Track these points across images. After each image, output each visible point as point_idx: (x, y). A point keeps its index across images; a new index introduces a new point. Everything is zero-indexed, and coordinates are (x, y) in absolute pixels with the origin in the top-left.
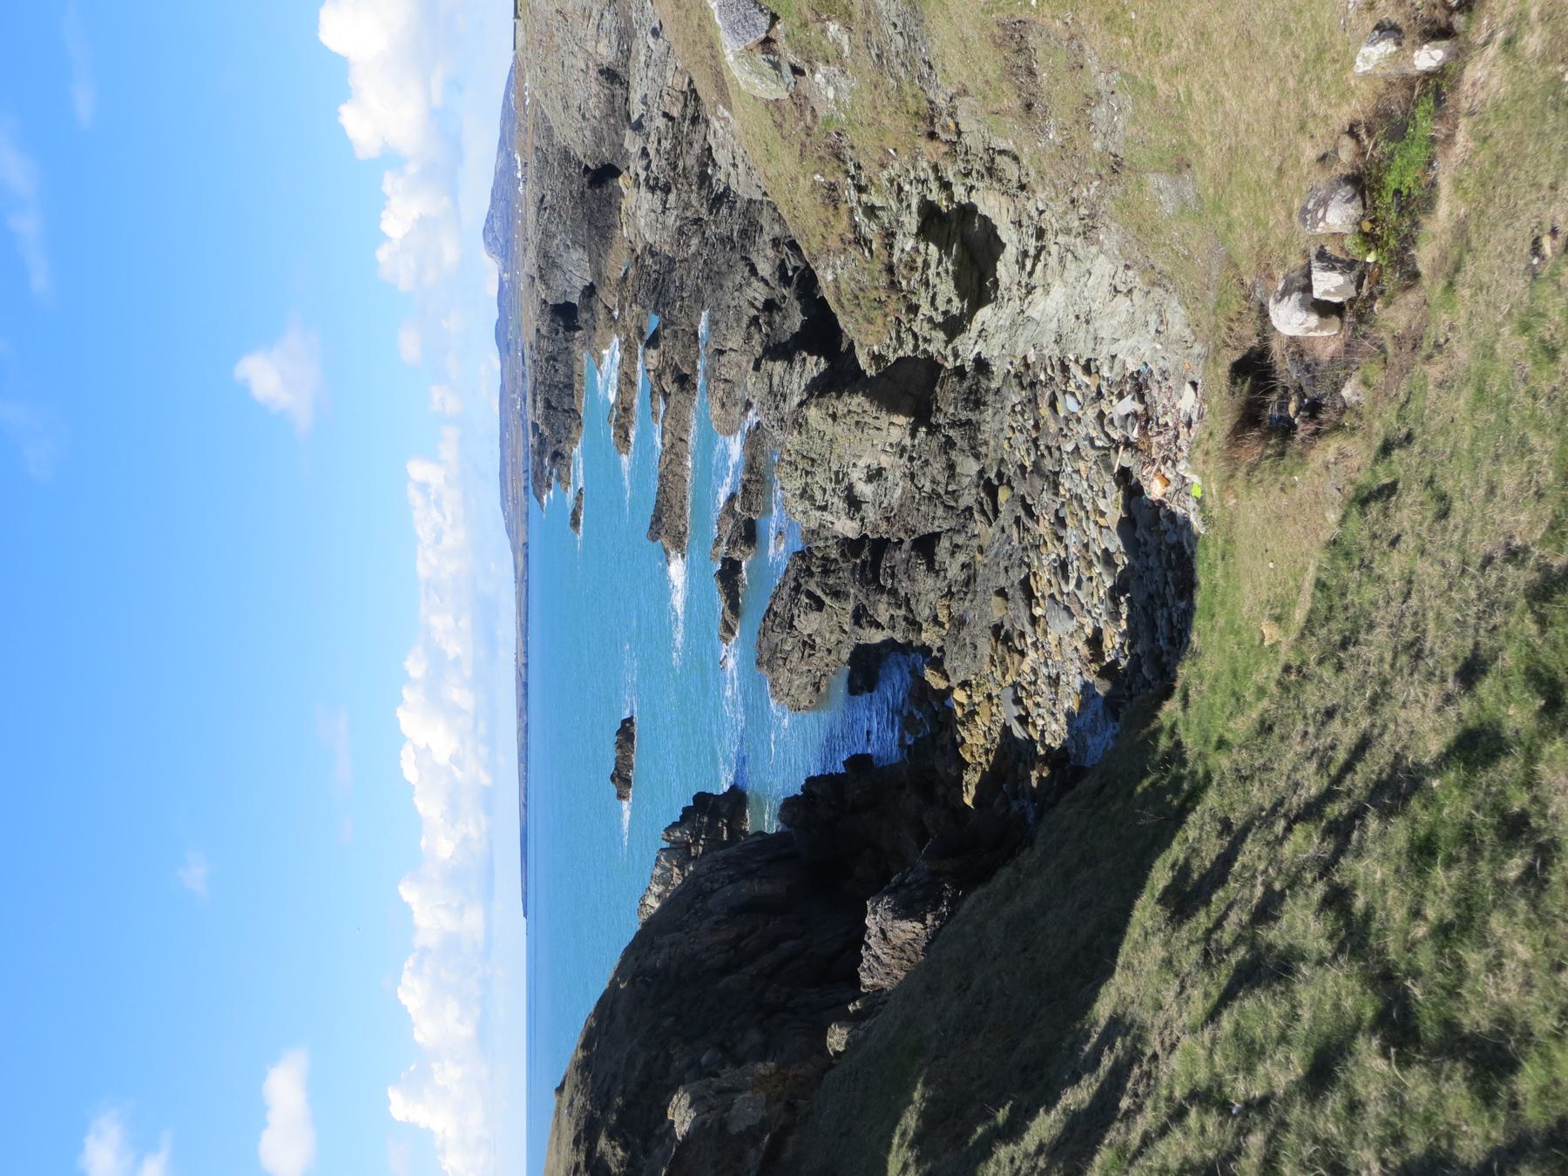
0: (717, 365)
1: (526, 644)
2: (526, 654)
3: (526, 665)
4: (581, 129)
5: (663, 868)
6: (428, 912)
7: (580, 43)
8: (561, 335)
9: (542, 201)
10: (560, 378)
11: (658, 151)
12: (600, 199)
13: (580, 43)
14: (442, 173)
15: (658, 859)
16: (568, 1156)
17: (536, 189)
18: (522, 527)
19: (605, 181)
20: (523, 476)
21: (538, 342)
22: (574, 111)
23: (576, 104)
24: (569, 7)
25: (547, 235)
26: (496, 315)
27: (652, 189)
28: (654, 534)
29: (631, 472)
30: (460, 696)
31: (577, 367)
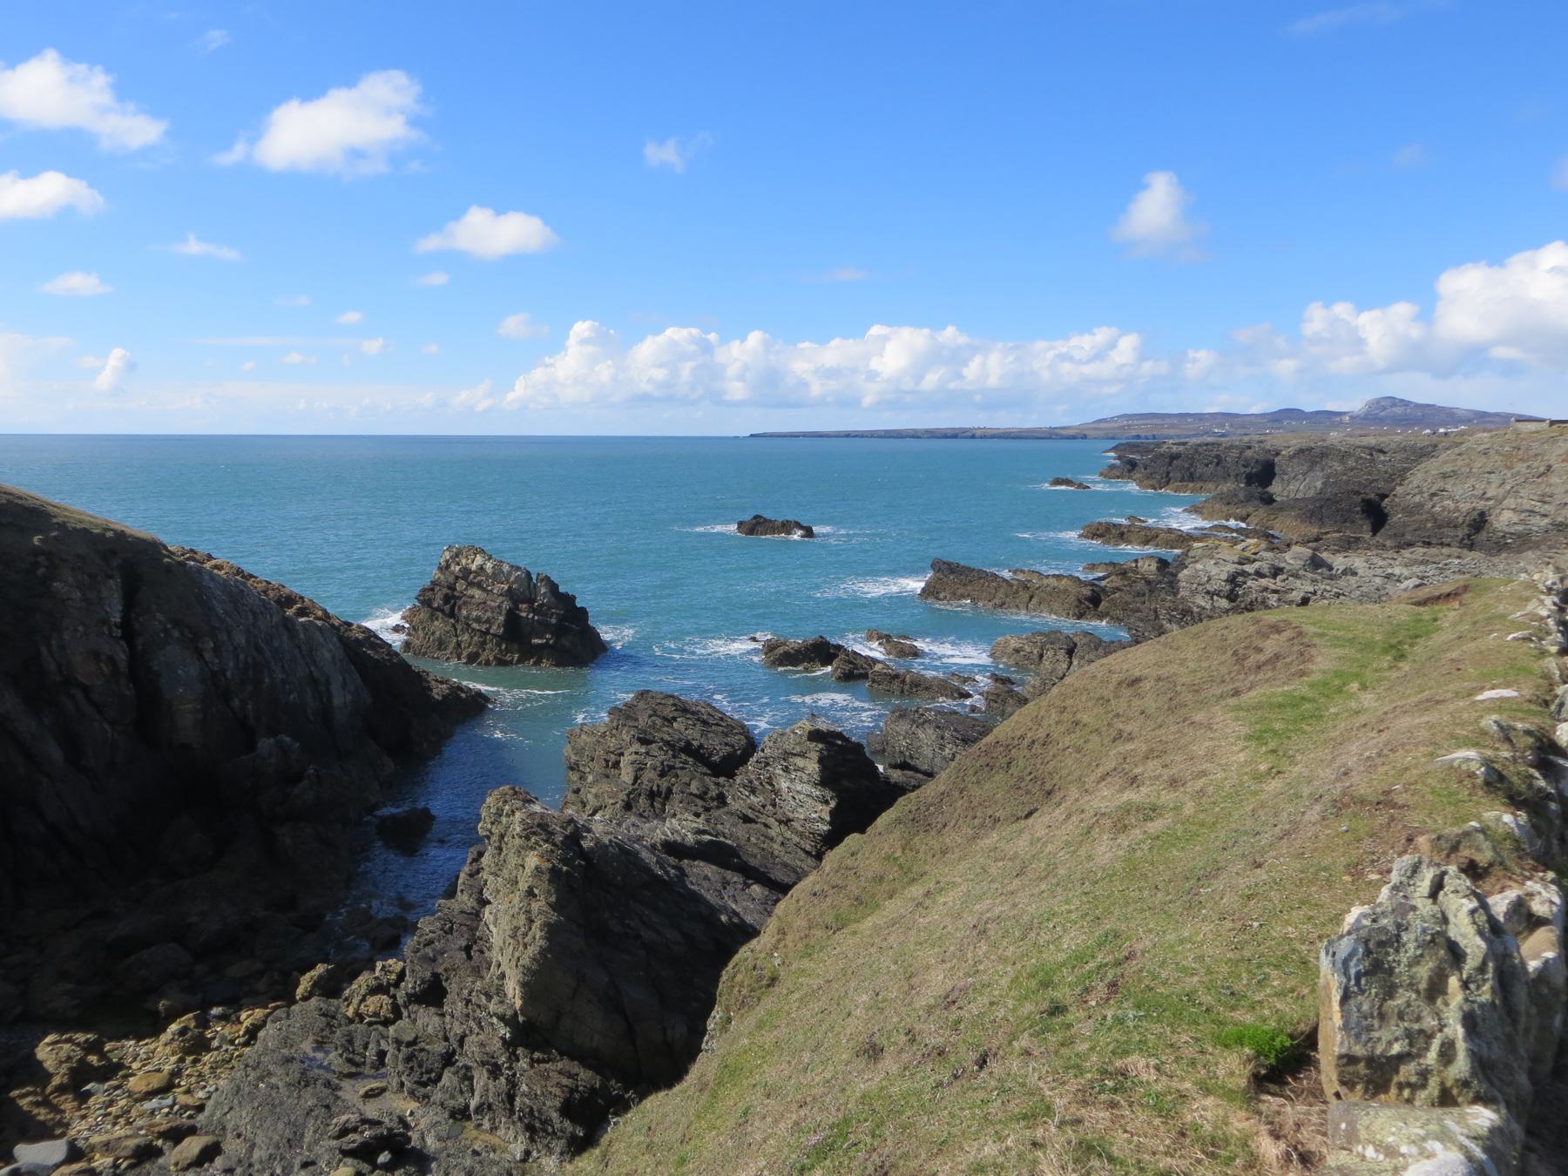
0: (1057, 646)
1: (993, 437)
2: (983, 437)
3: (973, 437)
4: (1421, 492)
5: (509, 573)
6: (744, 351)
7: (1514, 492)
9: (1382, 451)
11: (1266, 589)
12: (1349, 511)
13: (1514, 492)
15: (518, 568)
17: (1393, 446)
18: (1101, 433)
19: (1368, 517)
20: (1149, 434)
21: (1237, 447)
22: (1440, 484)
23: (1448, 487)
24: (1554, 479)
25: (1344, 456)
26: (1308, 409)
27: (1232, 580)
28: (937, 565)
29: (1060, 542)
30: (931, 380)
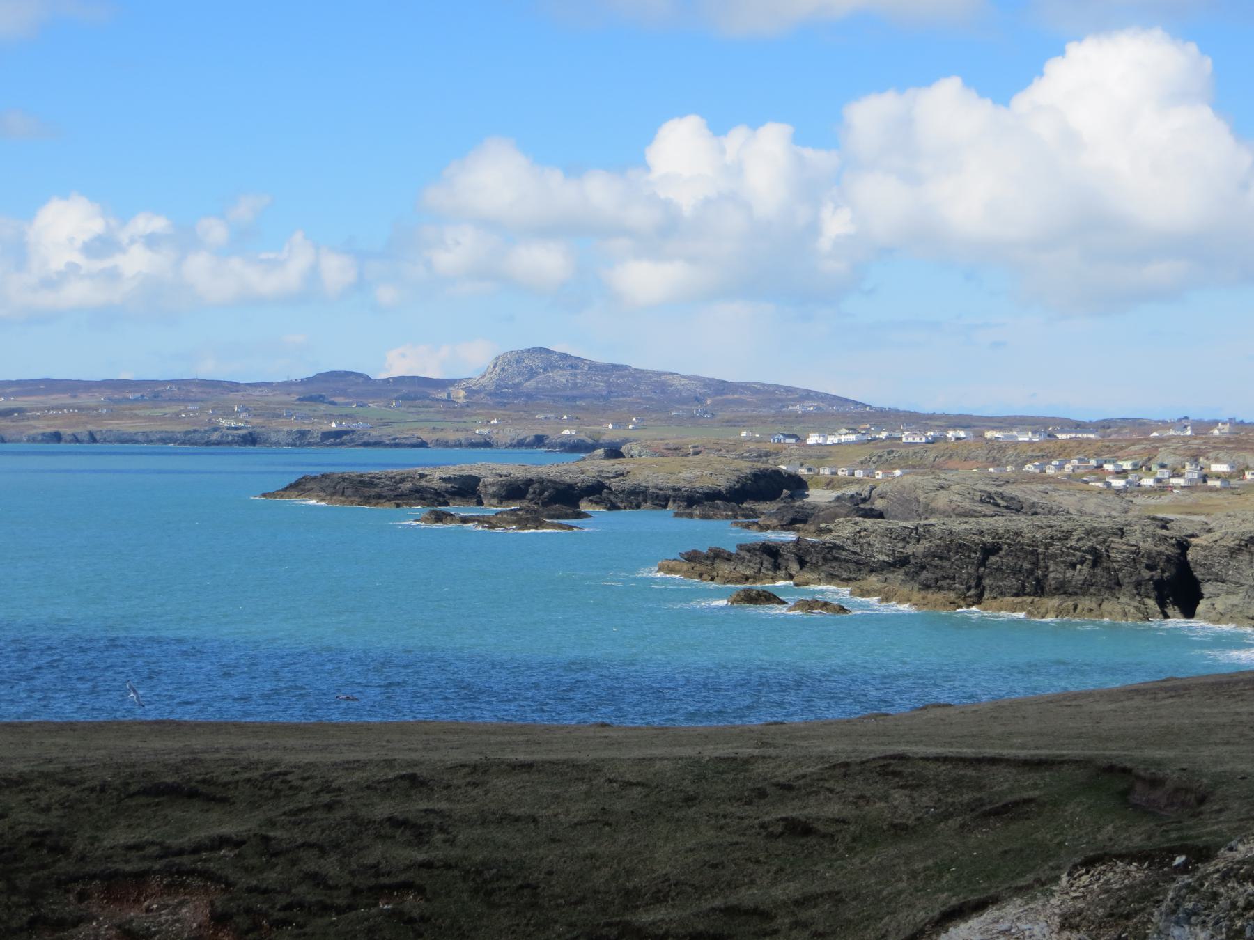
8: (1146, 574)
10: (1055, 574)
14: (778, 271)
16: (18, 759)
31: (1086, 603)
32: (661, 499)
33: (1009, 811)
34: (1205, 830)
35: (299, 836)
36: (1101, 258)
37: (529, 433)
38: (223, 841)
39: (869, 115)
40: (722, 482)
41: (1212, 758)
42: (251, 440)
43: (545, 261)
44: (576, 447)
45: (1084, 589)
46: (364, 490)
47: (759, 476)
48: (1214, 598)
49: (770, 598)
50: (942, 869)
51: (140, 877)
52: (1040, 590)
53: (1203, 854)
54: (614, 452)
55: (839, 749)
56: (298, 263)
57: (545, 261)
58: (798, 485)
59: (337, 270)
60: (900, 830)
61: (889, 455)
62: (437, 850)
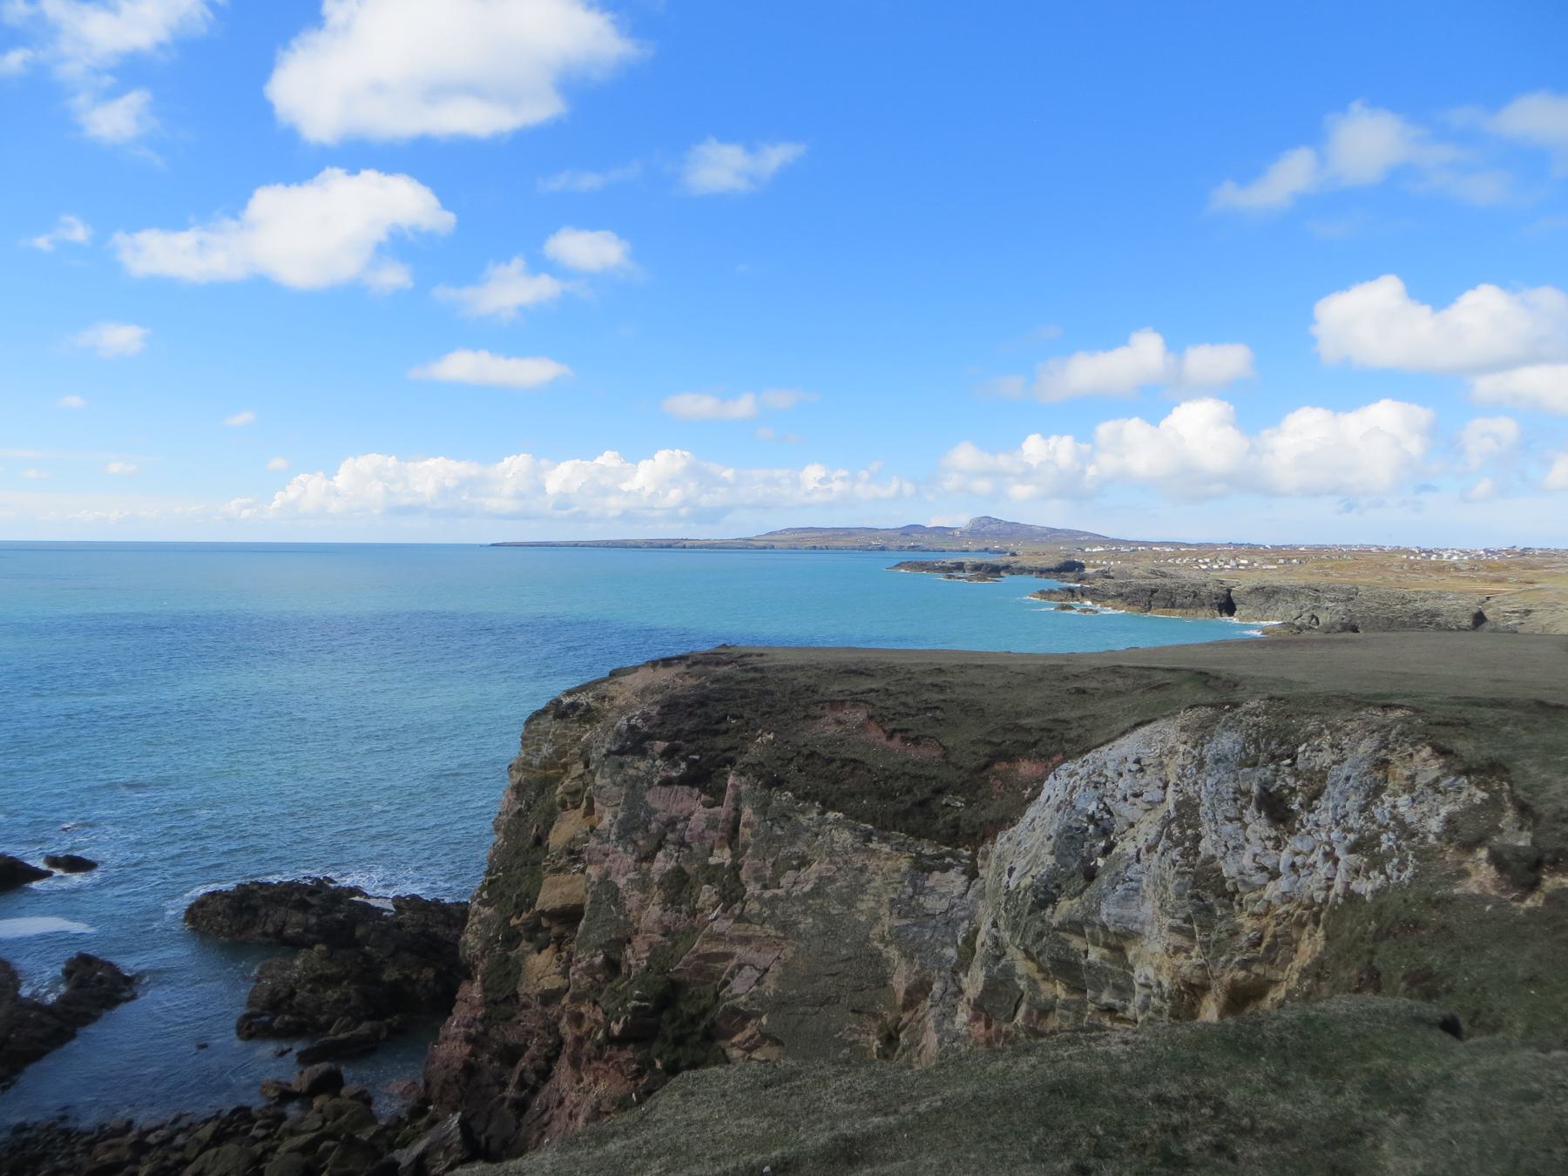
10: (1179, 600)
14: (1069, 488)
32: (1031, 572)
33: (1159, 687)
34: (1237, 697)
35: (899, 689)
36: (1191, 483)
37: (982, 547)
38: (872, 690)
39: (1105, 430)
40: (1053, 565)
41: (1240, 670)
42: (883, 549)
43: (983, 486)
44: (999, 552)
45: (1190, 606)
46: (922, 566)
47: (1067, 563)
48: (1241, 610)
49: (1071, 608)
50: (1135, 708)
51: (843, 702)
52: (1173, 606)
53: (1236, 705)
54: (1013, 554)
55: (1096, 663)
56: (895, 486)
57: (983, 486)
58: (1082, 566)
59: (908, 489)
60: (1118, 693)
61: (1116, 555)
62: (948, 695)
